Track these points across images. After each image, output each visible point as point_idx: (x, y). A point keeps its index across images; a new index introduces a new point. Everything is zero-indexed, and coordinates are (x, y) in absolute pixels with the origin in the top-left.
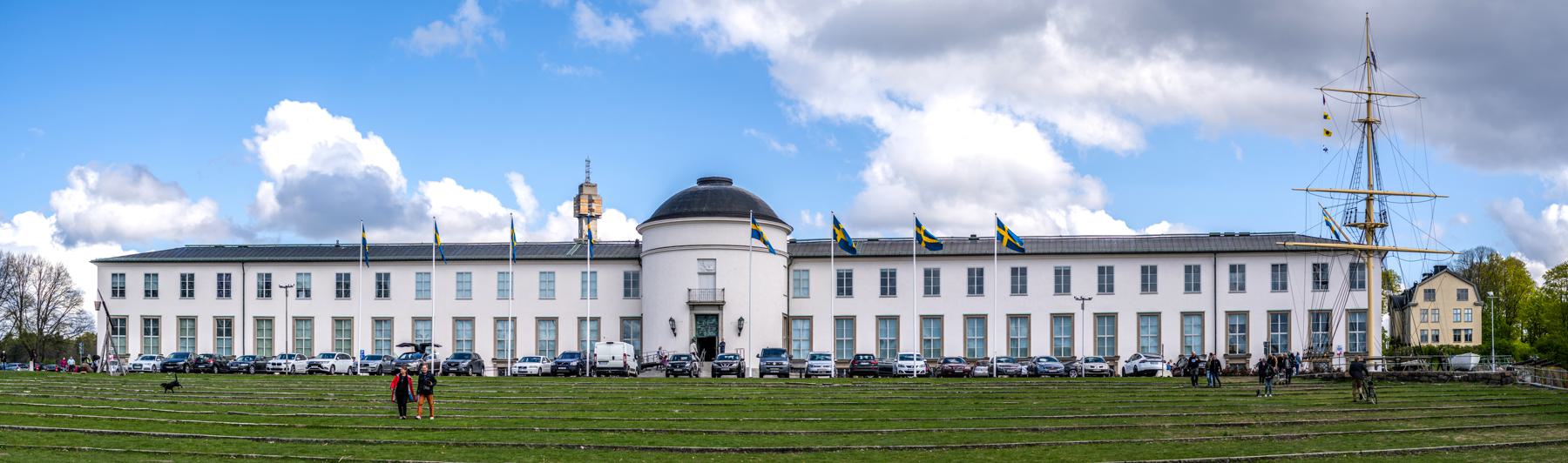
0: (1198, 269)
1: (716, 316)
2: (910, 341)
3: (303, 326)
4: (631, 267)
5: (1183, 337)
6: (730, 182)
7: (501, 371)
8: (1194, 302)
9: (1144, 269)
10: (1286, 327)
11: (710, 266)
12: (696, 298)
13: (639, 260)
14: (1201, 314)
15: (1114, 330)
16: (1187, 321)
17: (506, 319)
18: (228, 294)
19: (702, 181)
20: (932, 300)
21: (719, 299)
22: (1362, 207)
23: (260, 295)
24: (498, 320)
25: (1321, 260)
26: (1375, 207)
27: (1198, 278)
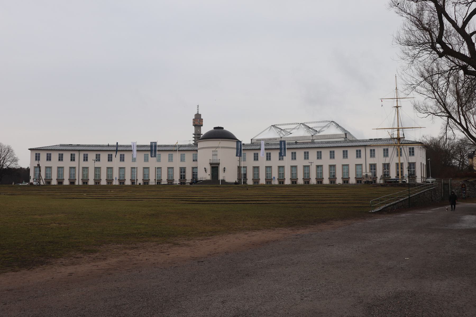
0: (360, 151)
1: (218, 167)
2: (379, 173)
3: (110, 170)
4: (195, 153)
5: (356, 172)
6: (223, 128)
7: (133, 183)
8: (359, 161)
9: (344, 151)
10: (388, 168)
11: (215, 153)
12: (211, 162)
13: (197, 150)
14: (361, 165)
15: (258, 171)
16: (121, 170)
17: (135, 168)
18: (74, 160)
19: (215, 128)
20: (332, 160)
21: (218, 162)
22: (396, 133)
23: (84, 160)
24: (132, 168)
25: (372, 148)
26: (401, 132)
27: (360, 154)
